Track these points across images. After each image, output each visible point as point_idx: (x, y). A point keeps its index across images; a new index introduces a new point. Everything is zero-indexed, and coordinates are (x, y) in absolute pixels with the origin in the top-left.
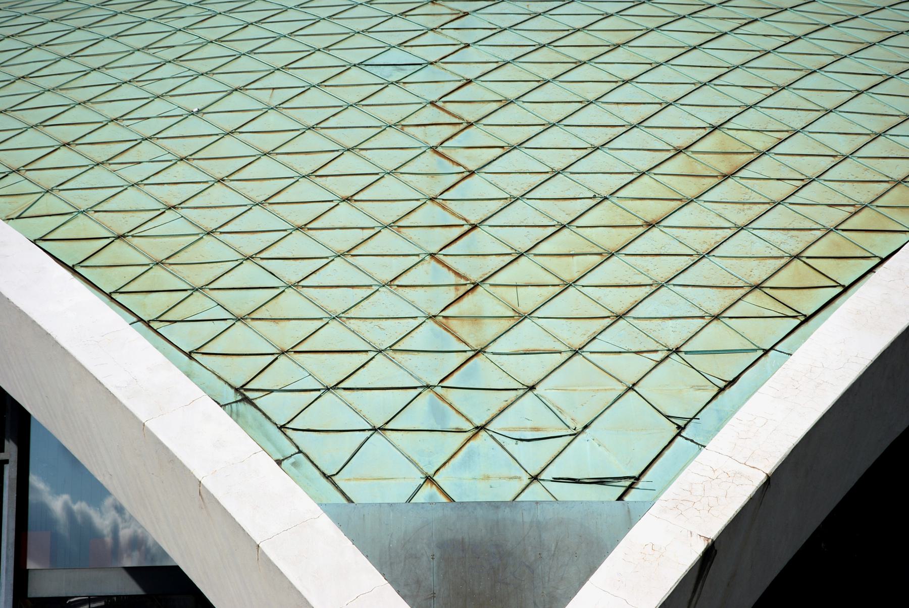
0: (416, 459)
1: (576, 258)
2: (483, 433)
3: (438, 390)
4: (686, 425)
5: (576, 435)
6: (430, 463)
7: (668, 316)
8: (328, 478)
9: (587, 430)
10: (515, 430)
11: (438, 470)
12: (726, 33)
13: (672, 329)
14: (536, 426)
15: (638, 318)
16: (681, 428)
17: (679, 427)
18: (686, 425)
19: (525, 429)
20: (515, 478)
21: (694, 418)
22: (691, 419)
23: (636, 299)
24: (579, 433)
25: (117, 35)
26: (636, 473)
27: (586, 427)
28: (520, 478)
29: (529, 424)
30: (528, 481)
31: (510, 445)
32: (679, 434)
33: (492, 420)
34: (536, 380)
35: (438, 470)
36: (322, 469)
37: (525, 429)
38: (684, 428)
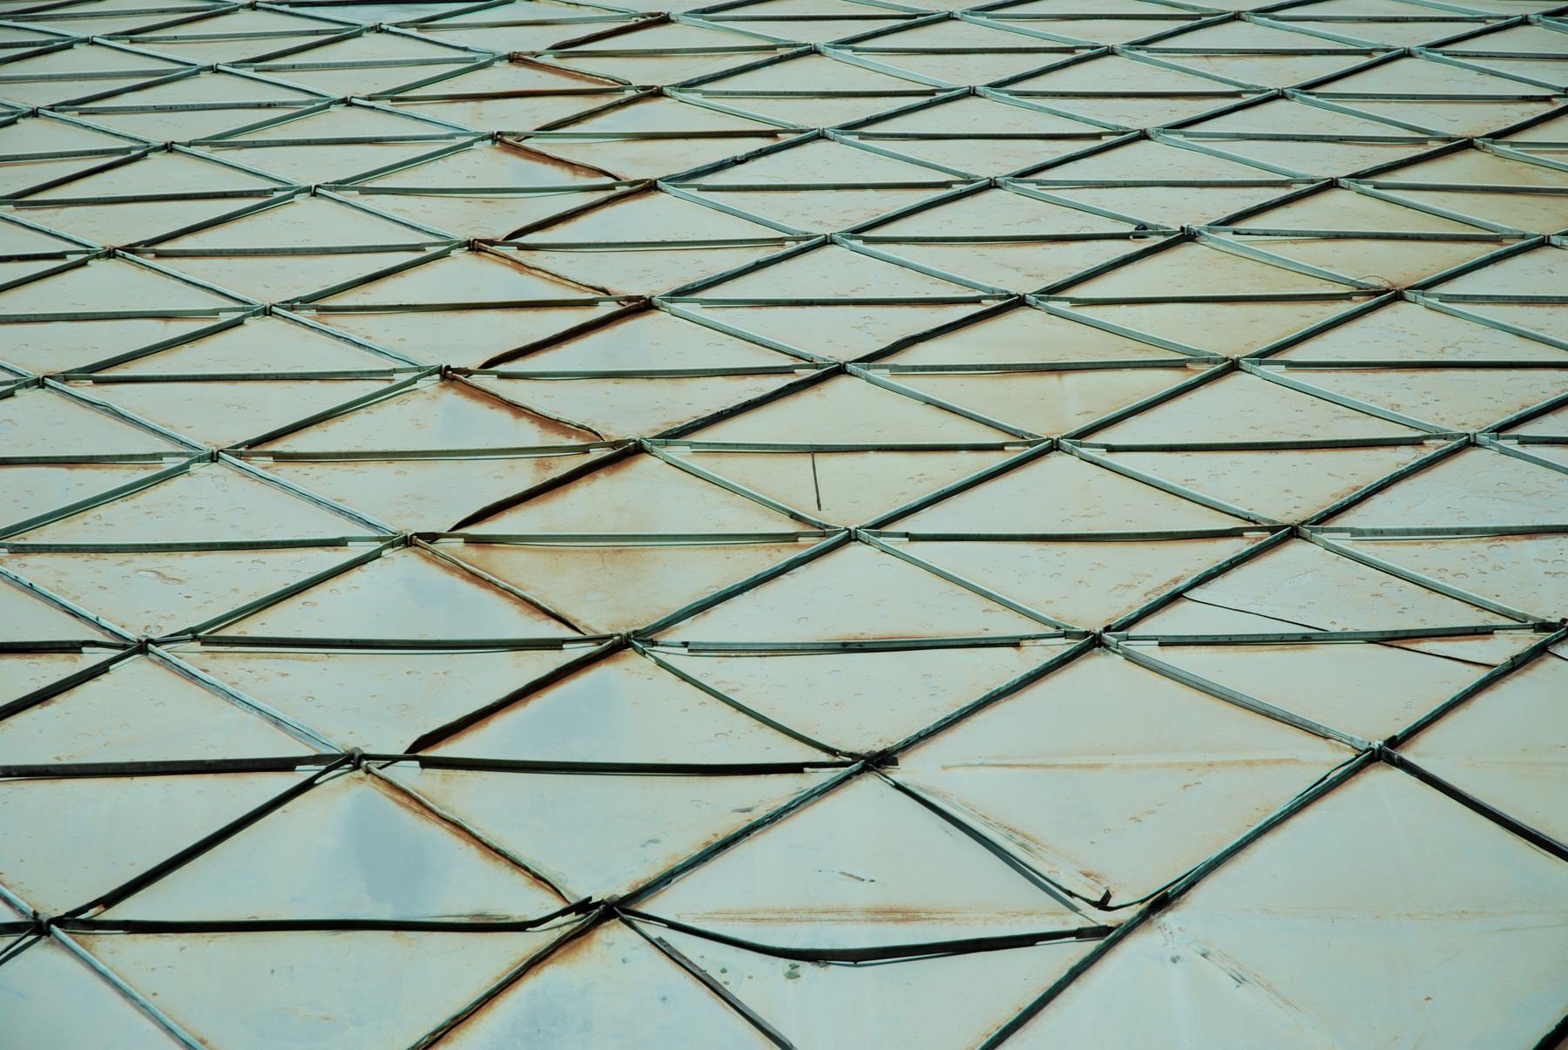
2: (614, 935)
3: (408, 774)
5: (1108, 938)
9: (1169, 918)
12: (840, 370)
15: (1361, 533)
19: (842, 914)
23: (1356, 482)
24: (1129, 929)
25: (95, 373)
27: (1161, 902)
29: (861, 896)
34: (898, 738)
37: (842, 914)
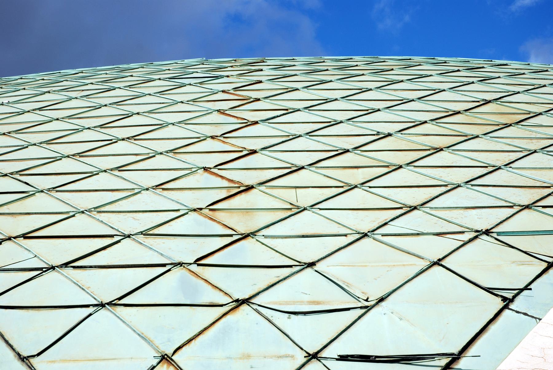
0: (150, 335)
1: (360, 170)
3: (194, 268)
4: (514, 297)
5: (368, 309)
6: (169, 341)
7: (470, 209)
8: (23, 359)
10: (287, 303)
11: (179, 348)
13: (476, 217)
14: (316, 299)
16: (507, 302)
17: (504, 299)
18: (514, 297)
19: (302, 303)
20: (287, 356)
21: (526, 288)
22: (521, 290)
26: (455, 350)
27: (382, 300)
28: (292, 357)
29: (306, 298)
30: (305, 359)
31: (281, 319)
32: (506, 307)
33: (258, 294)
35: (179, 348)
36: (18, 349)
37: (302, 303)
38: (512, 300)
